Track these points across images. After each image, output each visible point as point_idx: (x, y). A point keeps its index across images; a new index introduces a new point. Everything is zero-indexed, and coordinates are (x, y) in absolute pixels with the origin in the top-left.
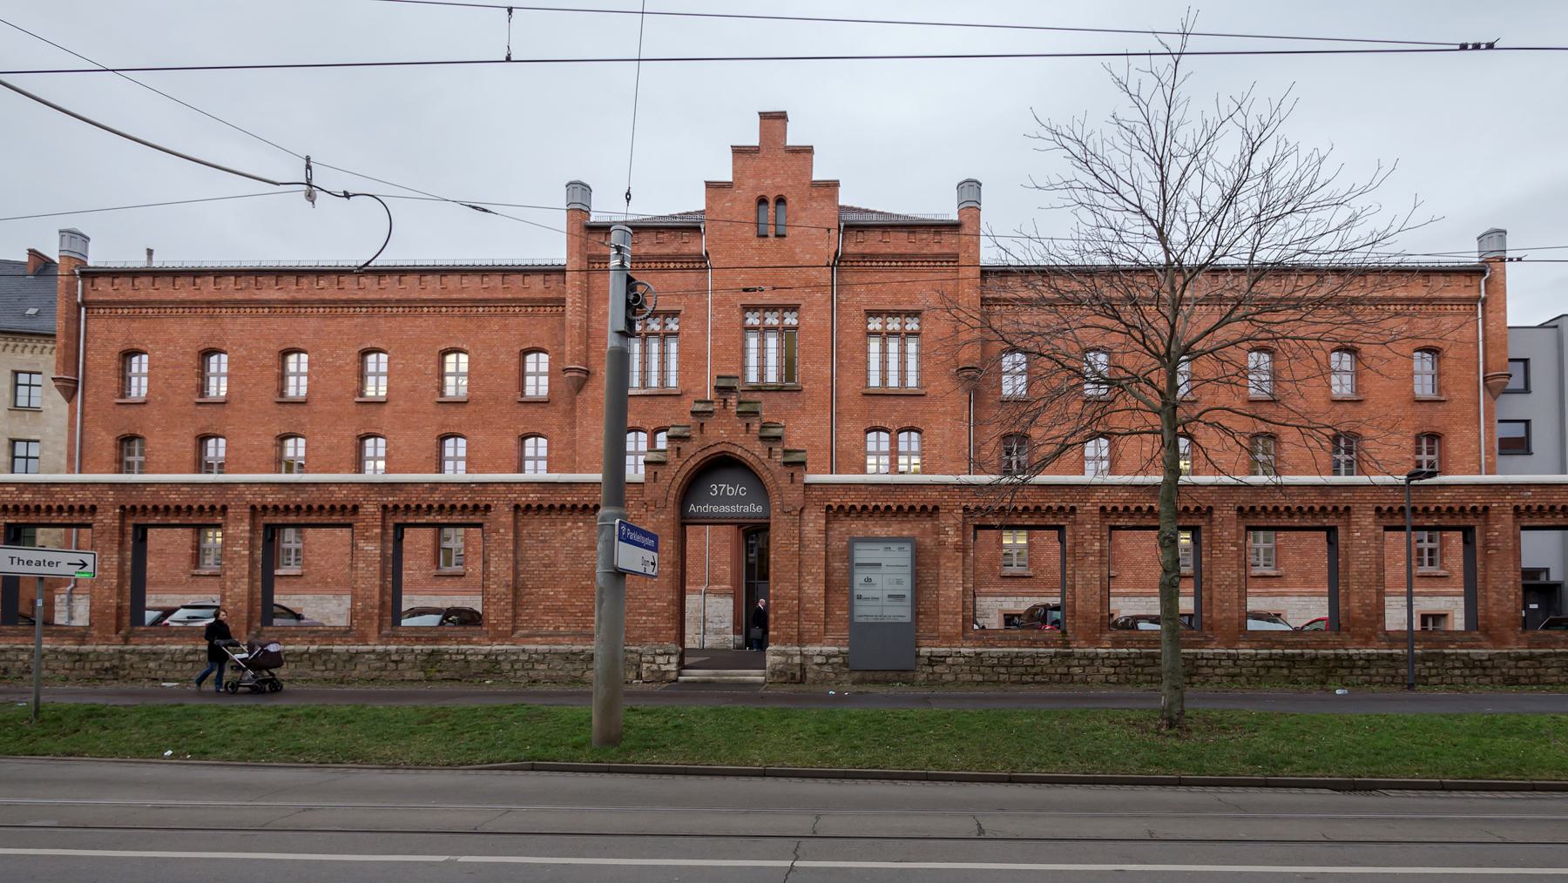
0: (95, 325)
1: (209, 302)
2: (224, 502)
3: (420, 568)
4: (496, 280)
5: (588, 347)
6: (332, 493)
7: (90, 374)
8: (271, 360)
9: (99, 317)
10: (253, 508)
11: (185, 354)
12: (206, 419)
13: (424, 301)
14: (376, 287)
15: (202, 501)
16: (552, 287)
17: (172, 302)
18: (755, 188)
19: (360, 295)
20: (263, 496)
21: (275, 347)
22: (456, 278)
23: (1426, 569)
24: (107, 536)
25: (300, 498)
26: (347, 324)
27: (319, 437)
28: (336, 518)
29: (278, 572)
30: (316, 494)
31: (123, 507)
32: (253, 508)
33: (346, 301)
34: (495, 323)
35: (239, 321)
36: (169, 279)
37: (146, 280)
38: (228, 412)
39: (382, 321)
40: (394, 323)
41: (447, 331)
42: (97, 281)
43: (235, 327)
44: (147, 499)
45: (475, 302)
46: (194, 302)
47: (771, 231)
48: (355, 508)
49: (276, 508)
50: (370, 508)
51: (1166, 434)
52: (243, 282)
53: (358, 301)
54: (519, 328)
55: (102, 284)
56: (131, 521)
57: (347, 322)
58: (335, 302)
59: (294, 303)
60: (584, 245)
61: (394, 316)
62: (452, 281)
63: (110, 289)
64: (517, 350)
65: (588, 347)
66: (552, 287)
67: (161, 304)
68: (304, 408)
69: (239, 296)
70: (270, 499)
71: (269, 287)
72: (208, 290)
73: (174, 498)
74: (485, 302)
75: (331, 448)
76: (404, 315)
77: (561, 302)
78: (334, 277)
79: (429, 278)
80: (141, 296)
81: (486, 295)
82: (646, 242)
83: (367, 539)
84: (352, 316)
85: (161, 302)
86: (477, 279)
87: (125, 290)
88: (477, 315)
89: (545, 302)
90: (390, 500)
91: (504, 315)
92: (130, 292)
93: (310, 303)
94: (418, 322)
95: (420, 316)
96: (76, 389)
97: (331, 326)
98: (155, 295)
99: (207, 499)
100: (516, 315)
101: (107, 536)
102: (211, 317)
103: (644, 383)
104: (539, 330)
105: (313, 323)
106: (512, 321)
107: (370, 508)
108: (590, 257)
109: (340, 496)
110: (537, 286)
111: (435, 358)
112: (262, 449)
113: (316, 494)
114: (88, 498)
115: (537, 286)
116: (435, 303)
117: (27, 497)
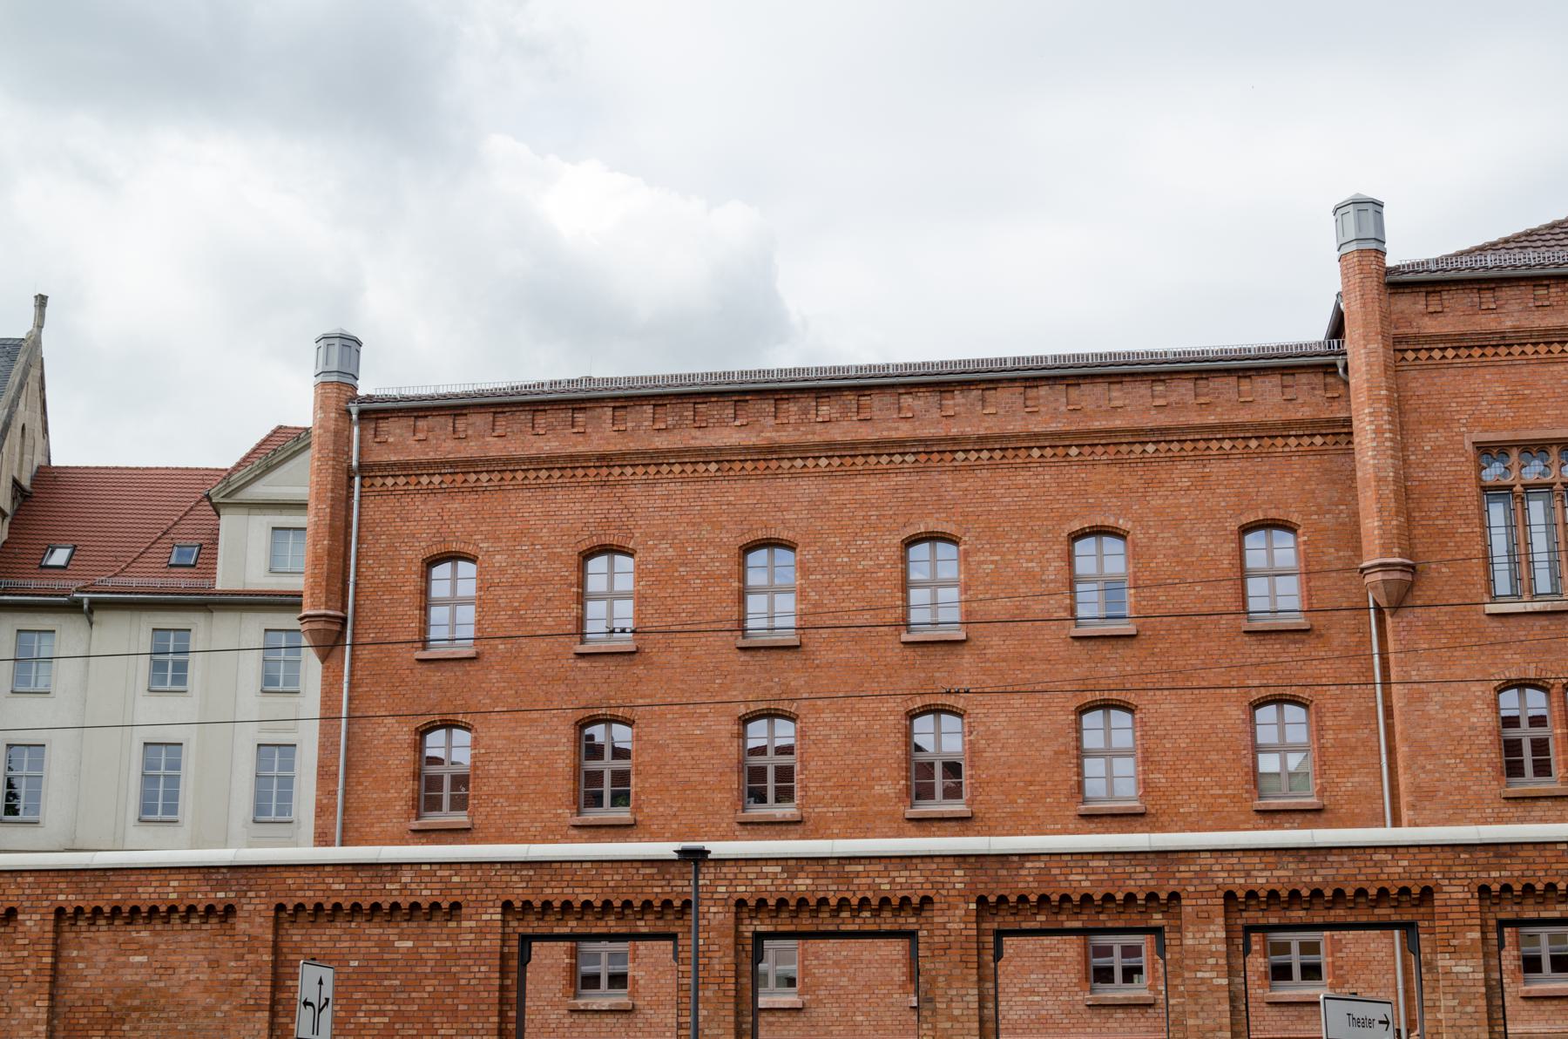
0: (379, 510)
1: (602, 457)
2: (1173, 885)
3: (1055, 990)
4: (1183, 390)
5: (1409, 518)
6: (1383, 863)
7: (367, 604)
8: (719, 561)
9: (387, 493)
10: (1230, 896)
11: (551, 557)
12: (595, 687)
15: (1131, 885)
16: (1307, 401)
17: (530, 459)
19: (904, 431)
20: (1248, 875)
21: (733, 538)
22: (1100, 389)
24: (955, 954)
25: (1309, 878)
26: (874, 488)
29: (763, 1001)
30: (1349, 868)
31: (981, 901)
32: (1230, 896)
33: (876, 444)
34: (1183, 474)
35: (659, 490)
36: (525, 417)
37: (480, 421)
38: (640, 670)
39: (947, 478)
40: (969, 482)
42: (383, 425)
43: (651, 503)
44: (1027, 882)
45: (1140, 436)
46: (571, 458)
48: (1427, 893)
49: (1273, 894)
50: (1455, 893)
53: (901, 443)
54: (1234, 482)
55: (395, 430)
56: (991, 925)
57: (875, 483)
59: (772, 451)
60: (1385, 317)
61: (972, 468)
62: (1089, 396)
63: (411, 441)
64: (1233, 526)
65: (1409, 518)
66: (1307, 401)
67: (505, 465)
68: (1255, 695)
69: (661, 442)
70: (1262, 880)
71: (722, 423)
72: (601, 435)
73: (1079, 882)
74: (1161, 434)
75: (854, 739)
76: (993, 466)
77: (1341, 431)
78: (850, 398)
79: (1043, 391)
80: (471, 450)
81: (1162, 420)
82: (1514, 306)
83: (1455, 952)
84: (886, 472)
85: (508, 461)
86: (1143, 389)
87: (441, 442)
88: (1144, 460)
89: (1313, 427)
90: (1495, 877)
91: (1202, 459)
92: (450, 444)
93: (802, 451)
94: (1021, 477)
95: (1026, 466)
96: (342, 633)
97: (845, 491)
98: (495, 448)
99: (1140, 880)
100: (1227, 457)
101: (955, 954)
102: (604, 484)
103: (1522, 583)
104: (1285, 481)
105: (807, 488)
106: (1216, 469)
107: (1455, 893)
108: (1398, 339)
109: (1396, 871)
110: (1268, 401)
111: (1060, 547)
112: (711, 744)
113: (1349, 868)
114: (913, 883)
115: (1268, 401)
116: (1058, 441)
117: (803, 884)
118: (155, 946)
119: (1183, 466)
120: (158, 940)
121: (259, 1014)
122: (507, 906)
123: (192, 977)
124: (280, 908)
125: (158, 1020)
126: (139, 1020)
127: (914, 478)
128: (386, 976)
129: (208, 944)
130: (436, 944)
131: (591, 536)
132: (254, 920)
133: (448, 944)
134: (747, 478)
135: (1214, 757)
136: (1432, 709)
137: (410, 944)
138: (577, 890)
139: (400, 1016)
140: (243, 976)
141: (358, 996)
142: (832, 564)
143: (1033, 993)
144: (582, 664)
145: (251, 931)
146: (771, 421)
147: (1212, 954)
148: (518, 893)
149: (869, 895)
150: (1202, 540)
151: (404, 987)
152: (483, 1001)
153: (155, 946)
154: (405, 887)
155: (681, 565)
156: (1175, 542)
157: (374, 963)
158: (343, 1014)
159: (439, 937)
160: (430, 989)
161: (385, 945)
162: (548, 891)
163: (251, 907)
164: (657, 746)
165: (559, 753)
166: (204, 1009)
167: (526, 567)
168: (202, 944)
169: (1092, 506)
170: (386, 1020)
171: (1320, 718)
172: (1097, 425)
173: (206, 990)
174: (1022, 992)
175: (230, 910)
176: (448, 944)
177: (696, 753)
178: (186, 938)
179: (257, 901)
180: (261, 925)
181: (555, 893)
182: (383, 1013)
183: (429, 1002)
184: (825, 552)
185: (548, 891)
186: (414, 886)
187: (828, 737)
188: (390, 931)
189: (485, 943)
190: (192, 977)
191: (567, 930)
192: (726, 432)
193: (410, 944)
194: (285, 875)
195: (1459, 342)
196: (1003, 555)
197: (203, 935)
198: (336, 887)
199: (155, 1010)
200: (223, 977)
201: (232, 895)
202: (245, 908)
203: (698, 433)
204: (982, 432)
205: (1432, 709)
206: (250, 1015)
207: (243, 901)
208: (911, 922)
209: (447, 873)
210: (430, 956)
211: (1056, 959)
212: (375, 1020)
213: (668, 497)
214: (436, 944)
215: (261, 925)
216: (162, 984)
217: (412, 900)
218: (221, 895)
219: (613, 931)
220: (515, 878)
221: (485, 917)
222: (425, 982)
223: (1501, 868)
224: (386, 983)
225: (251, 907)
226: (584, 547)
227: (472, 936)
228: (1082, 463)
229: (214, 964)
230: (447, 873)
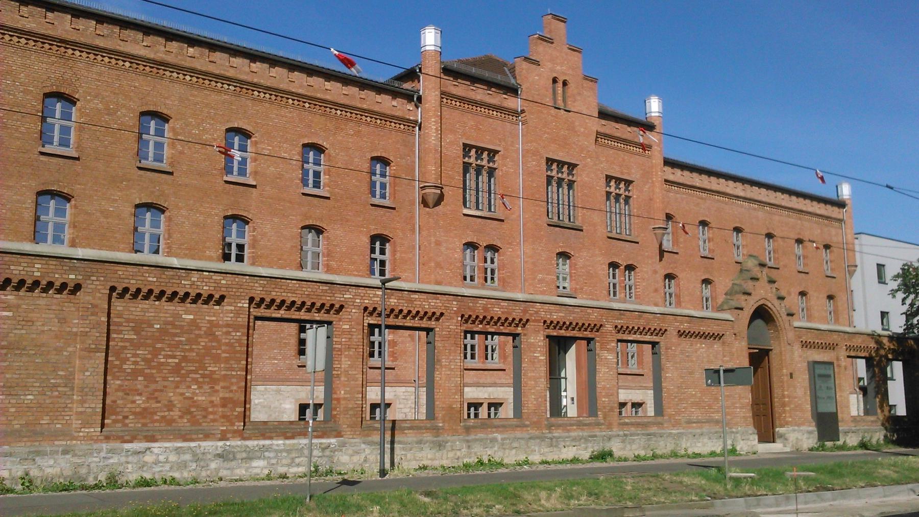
6: (589, 314)
13: (291, 93)
14: (247, 69)
18: (552, 70)
21: (139, 107)
23: (476, 363)
27: (184, 212)
28: (282, 313)
34: (351, 128)
35: (94, 69)
39: (249, 103)
41: (310, 126)
47: (560, 84)
51: (294, 455)
52: (105, 29)
57: (214, 97)
58: (206, 74)
61: (261, 101)
71: (136, 42)
84: (220, 92)
94: (284, 111)
95: (286, 106)
102: (62, 57)
105: (178, 89)
106: (364, 129)
118: (18, 306)
119: (351, 124)
120: (20, 302)
121: (98, 354)
122: (251, 300)
123: (46, 328)
124: (113, 289)
125: (21, 355)
126: (6, 354)
127: (233, 98)
128: (176, 335)
129: (58, 308)
130: (207, 318)
131: (52, 85)
132: (95, 292)
133: (214, 318)
134: (146, 75)
135: (356, 257)
136: (443, 249)
137: (192, 317)
138: (289, 295)
139: (184, 359)
140: (88, 330)
141: (159, 346)
142: (190, 133)
143: (275, 359)
144: (43, 158)
145: (93, 301)
146: (163, 48)
147: (539, 346)
148: (258, 293)
149: (420, 310)
150: (356, 160)
151: (189, 342)
152: (237, 352)
153: (18, 306)
154: (193, 283)
155: (107, 114)
156: (346, 158)
157: (170, 327)
158: (149, 356)
159: (211, 314)
160: (203, 344)
161: (177, 316)
162: (274, 293)
163: (93, 286)
164: (87, 213)
165: (26, 208)
166: (55, 349)
167: (9, 94)
168: (54, 307)
169: (312, 133)
170: (177, 361)
171: (395, 247)
172: (319, 95)
173: (56, 337)
174: (270, 358)
175: (78, 287)
176: (214, 318)
177: (110, 220)
178: (42, 302)
179: (98, 283)
180: (100, 298)
181: (278, 295)
182: (174, 357)
183: (203, 351)
184: (187, 126)
185: (274, 293)
186: (199, 283)
187: (184, 223)
188: (179, 308)
189: (239, 319)
190: (46, 328)
191: (279, 316)
192: (137, 47)
193: (192, 317)
194: (117, 268)
195: (462, 99)
196: (273, 147)
197: (55, 301)
198: (151, 279)
199: (18, 349)
200: (68, 329)
201: (81, 277)
202: (88, 286)
203: (122, 43)
204: (269, 85)
205: (443, 249)
206: (92, 354)
207: (89, 282)
208: (433, 324)
209: (219, 278)
210: (204, 326)
211: (285, 343)
212: (170, 361)
213: (100, 74)
214: (207, 318)
215: (100, 298)
216: (23, 332)
217: (198, 291)
218: (72, 277)
219: (302, 318)
220: (256, 285)
221: (239, 305)
222: (200, 340)
223: (621, 319)
224: (177, 339)
225: (93, 286)
226: (47, 90)
227: (232, 315)
228: (310, 112)
229: (63, 321)
230: (219, 278)
